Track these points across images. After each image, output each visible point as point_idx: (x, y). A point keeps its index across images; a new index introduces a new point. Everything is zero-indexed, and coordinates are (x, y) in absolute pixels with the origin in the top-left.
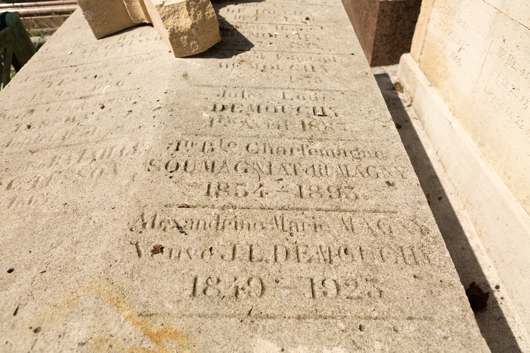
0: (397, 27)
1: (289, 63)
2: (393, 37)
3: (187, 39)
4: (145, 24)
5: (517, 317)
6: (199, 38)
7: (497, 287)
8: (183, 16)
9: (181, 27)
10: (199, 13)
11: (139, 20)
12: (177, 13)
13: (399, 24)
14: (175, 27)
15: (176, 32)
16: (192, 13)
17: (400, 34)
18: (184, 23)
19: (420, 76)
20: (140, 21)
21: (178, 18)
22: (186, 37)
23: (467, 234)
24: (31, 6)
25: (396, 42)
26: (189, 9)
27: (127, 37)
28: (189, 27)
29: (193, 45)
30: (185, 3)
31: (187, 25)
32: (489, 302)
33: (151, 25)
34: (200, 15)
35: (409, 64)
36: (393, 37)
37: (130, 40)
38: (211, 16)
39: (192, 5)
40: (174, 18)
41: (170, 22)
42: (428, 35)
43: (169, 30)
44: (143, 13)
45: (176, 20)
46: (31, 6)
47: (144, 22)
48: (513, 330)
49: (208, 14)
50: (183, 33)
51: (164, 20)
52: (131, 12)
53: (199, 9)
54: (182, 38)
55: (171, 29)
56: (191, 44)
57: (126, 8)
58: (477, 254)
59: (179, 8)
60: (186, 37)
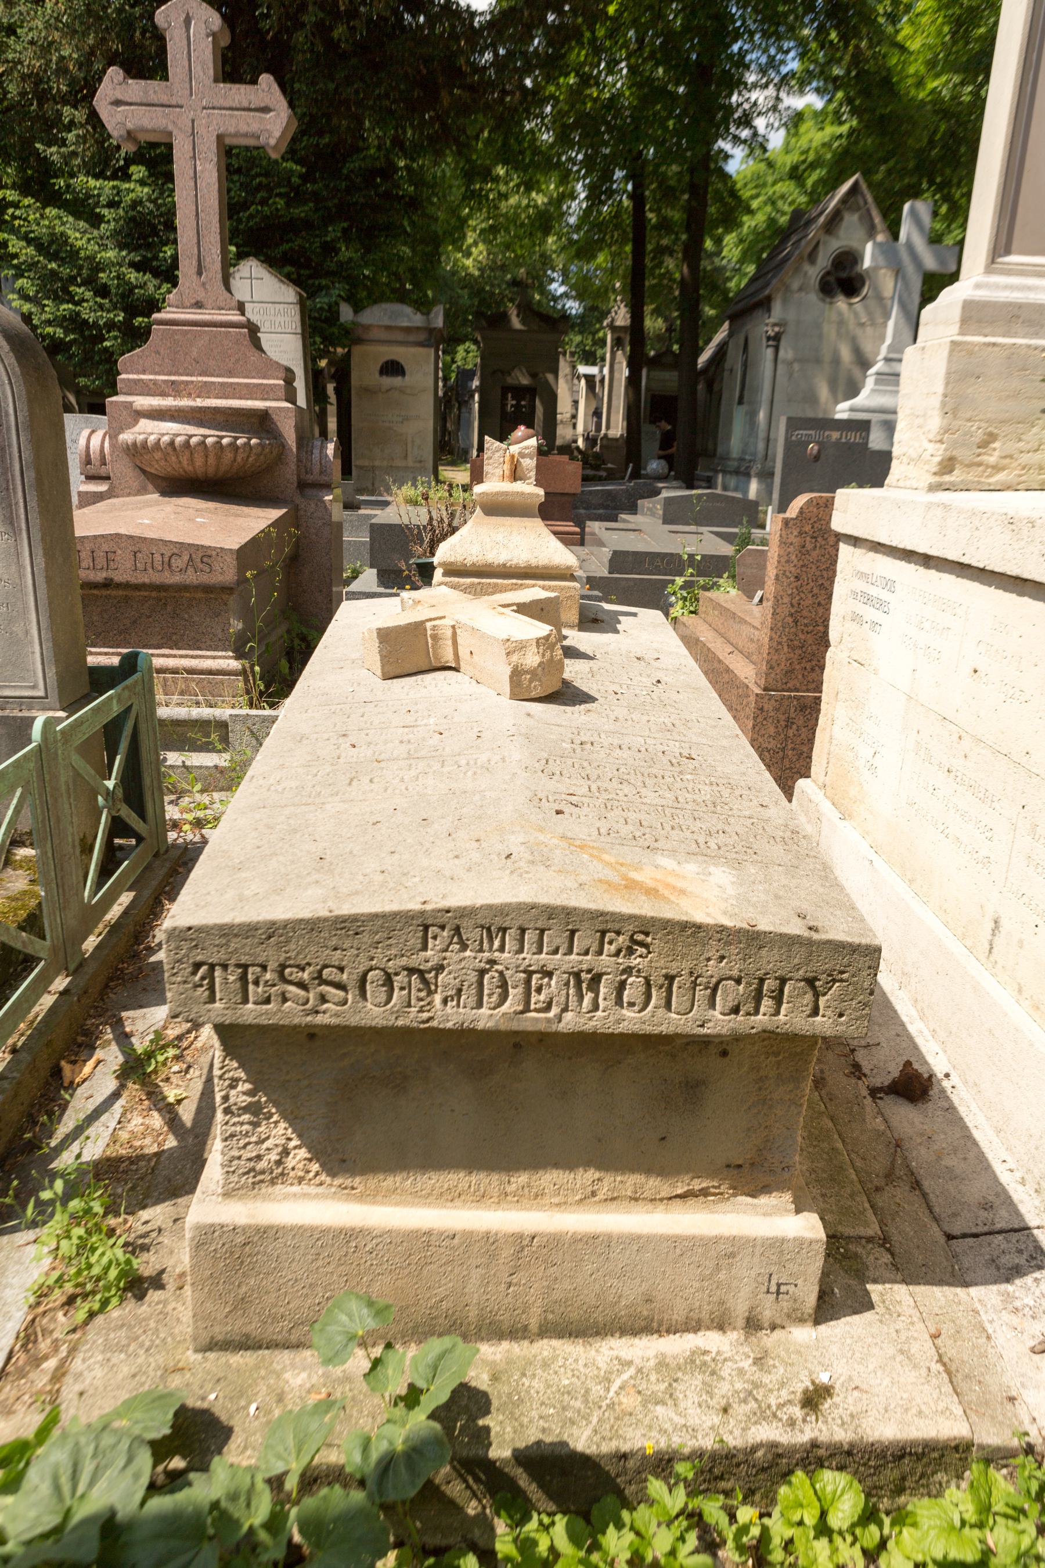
0: (787, 737)
1: (645, 718)
2: (781, 754)
4: (450, 668)
5: (974, 1107)
6: (544, 679)
7: (947, 1075)
13: (790, 733)
17: (793, 749)
19: (826, 807)
23: (904, 1018)
24: (106, 654)
25: (786, 762)
26: (538, 646)
32: (933, 1092)
34: (548, 654)
35: (810, 792)
36: (781, 754)
41: (515, 658)
42: (834, 742)
46: (106, 654)
48: (966, 1120)
58: (919, 1041)
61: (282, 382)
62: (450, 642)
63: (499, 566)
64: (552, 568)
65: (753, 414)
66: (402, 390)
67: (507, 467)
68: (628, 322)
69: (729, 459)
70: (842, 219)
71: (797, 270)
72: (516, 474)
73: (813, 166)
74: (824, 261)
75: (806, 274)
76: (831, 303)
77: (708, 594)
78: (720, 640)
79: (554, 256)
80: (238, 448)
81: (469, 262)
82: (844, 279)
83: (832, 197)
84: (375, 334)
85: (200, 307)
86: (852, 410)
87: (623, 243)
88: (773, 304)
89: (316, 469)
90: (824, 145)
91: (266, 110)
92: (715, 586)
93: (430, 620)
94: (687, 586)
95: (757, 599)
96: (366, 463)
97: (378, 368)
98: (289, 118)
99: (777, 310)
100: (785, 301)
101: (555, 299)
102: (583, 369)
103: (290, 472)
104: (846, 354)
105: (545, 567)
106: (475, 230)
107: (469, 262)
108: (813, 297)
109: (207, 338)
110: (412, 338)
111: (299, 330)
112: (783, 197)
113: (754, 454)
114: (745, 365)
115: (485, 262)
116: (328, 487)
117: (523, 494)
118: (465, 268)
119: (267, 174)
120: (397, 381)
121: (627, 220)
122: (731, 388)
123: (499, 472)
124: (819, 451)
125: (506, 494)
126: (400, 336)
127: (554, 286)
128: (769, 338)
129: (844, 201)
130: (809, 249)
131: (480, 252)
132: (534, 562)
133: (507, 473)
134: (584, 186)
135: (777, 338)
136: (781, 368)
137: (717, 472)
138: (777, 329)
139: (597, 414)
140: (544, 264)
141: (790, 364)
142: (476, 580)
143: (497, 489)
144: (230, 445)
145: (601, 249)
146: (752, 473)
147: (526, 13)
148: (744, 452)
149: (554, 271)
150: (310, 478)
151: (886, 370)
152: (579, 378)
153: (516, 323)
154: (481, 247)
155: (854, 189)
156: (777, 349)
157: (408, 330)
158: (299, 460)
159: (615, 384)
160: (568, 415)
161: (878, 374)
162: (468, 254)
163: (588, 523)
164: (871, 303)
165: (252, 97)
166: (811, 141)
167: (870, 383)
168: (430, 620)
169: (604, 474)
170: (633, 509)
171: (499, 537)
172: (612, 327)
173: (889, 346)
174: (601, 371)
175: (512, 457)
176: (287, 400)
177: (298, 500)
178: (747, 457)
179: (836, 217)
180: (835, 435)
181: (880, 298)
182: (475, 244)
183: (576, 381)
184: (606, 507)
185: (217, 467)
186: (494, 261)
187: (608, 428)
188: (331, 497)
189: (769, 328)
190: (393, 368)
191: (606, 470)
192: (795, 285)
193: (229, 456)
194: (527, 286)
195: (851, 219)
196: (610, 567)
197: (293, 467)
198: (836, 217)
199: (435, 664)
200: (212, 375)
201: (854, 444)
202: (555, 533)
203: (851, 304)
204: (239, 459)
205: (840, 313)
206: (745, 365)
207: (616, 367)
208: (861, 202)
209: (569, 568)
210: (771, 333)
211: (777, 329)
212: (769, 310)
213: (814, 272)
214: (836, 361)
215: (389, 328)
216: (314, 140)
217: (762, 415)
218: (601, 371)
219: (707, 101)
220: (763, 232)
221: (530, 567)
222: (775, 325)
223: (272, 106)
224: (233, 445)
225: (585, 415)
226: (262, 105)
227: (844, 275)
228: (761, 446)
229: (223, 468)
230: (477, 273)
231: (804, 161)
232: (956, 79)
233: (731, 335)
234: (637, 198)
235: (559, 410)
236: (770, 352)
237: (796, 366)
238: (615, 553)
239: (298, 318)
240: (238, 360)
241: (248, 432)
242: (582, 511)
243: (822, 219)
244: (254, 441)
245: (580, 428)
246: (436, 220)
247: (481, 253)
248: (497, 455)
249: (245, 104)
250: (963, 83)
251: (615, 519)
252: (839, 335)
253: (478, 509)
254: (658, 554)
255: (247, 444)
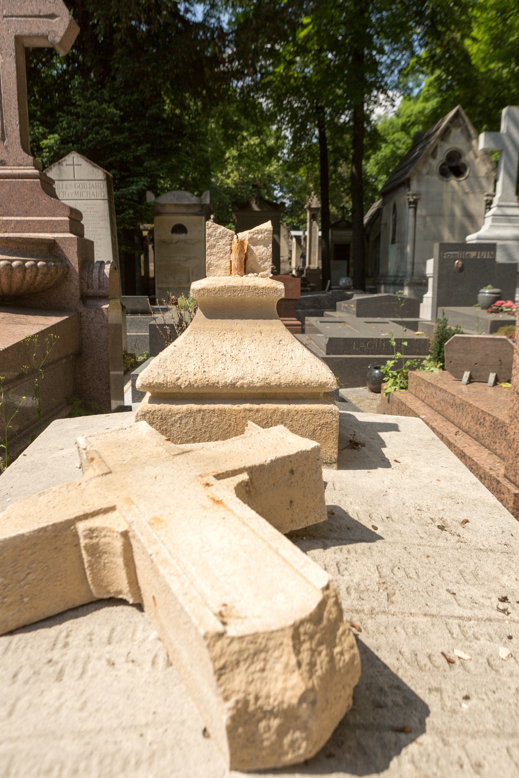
3: (280, 727)
4: (123, 602)
8: (279, 667)
9: (268, 697)
10: (320, 653)
11: (109, 592)
12: (262, 656)
14: (251, 698)
15: (252, 708)
16: (305, 656)
18: (280, 685)
20: (112, 595)
21: (263, 670)
22: (275, 723)
27: (76, 640)
28: (295, 701)
29: (293, 743)
30: (290, 632)
31: (289, 694)
33: (140, 607)
34: (322, 659)
37: (83, 654)
38: (347, 657)
39: (305, 633)
40: (252, 668)
41: (238, 680)
43: (231, 703)
44: (126, 581)
45: (257, 675)
47: (120, 596)
49: (342, 653)
50: (271, 712)
51: (220, 676)
52: (94, 575)
53: (320, 643)
54: (262, 725)
55: (237, 702)
56: (287, 741)
57: (86, 565)
59: (271, 644)
60: (275, 723)
61: (67, 219)
62: (120, 561)
63: (225, 386)
64: (300, 386)
65: (402, 250)
66: (185, 242)
67: (234, 257)
68: (319, 206)
69: (387, 276)
70: (450, 132)
71: (425, 162)
72: (246, 266)
73: (414, 124)
74: (441, 157)
75: (430, 164)
76: (447, 181)
77: (414, 373)
78: (438, 417)
79: (275, 176)
80: (25, 269)
81: (229, 181)
82: (455, 167)
83: (443, 121)
84: (169, 209)
85: (4, 165)
86: (478, 239)
87: (314, 161)
88: (411, 183)
89: (96, 284)
90: (420, 112)
91: (52, 16)
92: (420, 366)
93: (86, 517)
94: (398, 366)
95: (465, 379)
96: (164, 286)
97: (171, 229)
98: (71, 21)
99: (414, 186)
100: (419, 181)
101: (277, 199)
102: (294, 233)
103: (74, 287)
104: (458, 211)
105: (289, 386)
106: (232, 165)
107: (229, 181)
108: (436, 178)
109: (8, 187)
110: (191, 211)
111: (106, 197)
112: (399, 140)
113: (405, 272)
114: (395, 221)
115: (238, 181)
116: (105, 298)
117: (256, 288)
118: (228, 184)
119: (99, 116)
120: (182, 236)
121: (317, 150)
122: (387, 234)
123: (225, 263)
124: (463, 265)
125: (233, 289)
126: (183, 210)
127: (276, 192)
128: (410, 203)
129: (451, 121)
130: (432, 150)
131: (235, 176)
132: (274, 380)
133: (235, 263)
134: (291, 132)
135: (415, 202)
136: (419, 221)
137: (380, 284)
138: (415, 197)
139: (303, 256)
140: (270, 181)
141: (424, 217)
142: (195, 407)
143: (222, 284)
144: (18, 266)
145: (301, 166)
146: (405, 283)
147: (254, 22)
148: (398, 271)
149: (275, 184)
150: (91, 292)
151: (499, 212)
152: (292, 238)
153: (256, 208)
154: (235, 173)
155: (457, 115)
156: (415, 209)
157: (188, 206)
158: (82, 278)
159: (313, 239)
160: (287, 258)
161: (494, 215)
162: (228, 177)
163: (307, 318)
164: (472, 180)
165: (42, 7)
166: (412, 111)
167: (488, 221)
168: (86, 517)
169: (309, 289)
170: (333, 308)
171: (227, 347)
172: (310, 208)
173: (500, 198)
174: (304, 233)
175: (241, 243)
176: (71, 232)
177: (81, 309)
178: (400, 274)
179: (446, 133)
180: (473, 254)
181: (477, 177)
182: (232, 171)
183: (290, 240)
184: (315, 308)
185: (10, 286)
186: (243, 180)
187: (310, 263)
188: (107, 306)
189: (410, 197)
190: (180, 229)
191: (310, 287)
192: (424, 171)
193: (18, 276)
194: (260, 188)
195: (456, 132)
196: (328, 349)
197: (77, 283)
198: (447, 131)
199: (97, 594)
200: (13, 215)
201: (486, 259)
202: (286, 325)
203: (459, 181)
204: (28, 278)
205: (452, 187)
206: (395, 221)
207: (313, 230)
208: (462, 122)
209: (322, 385)
210: (411, 200)
211: (415, 197)
212: (409, 186)
213: (435, 164)
214: (452, 215)
215: (176, 205)
216: (128, 97)
217: (409, 249)
218: (304, 233)
219: (360, 79)
220: (389, 158)
221: (268, 386)
222: (414, 195)
223: (57, 13)
224: (22, 267)
225: (296, 257)
226: (50, 13)
227: (454, 164)
228: (409, 267)
229: (15, 286)
230: (233, 187)
231: (409, 121)
232: (500, 65)
233: (384, 204)
234: (322, 138)
235: (281, 255)
236: (411, 211)
237: (428, 219)
238: (331, 339)
239: (105, 189)
240: (32, 203)
241: (37, 257)
242: (300, 311)
243: (438, 132)
244: (40, 264)
245: (294, 265)
246: (207, 152)
247: (235, 176)
248: (222, 242)
249: (36, 12)
250: (503, 67)
251: (322, 315)
252: (453, 200)
253: (199, 311)
254: (362, 340)
255: (35, 265)
